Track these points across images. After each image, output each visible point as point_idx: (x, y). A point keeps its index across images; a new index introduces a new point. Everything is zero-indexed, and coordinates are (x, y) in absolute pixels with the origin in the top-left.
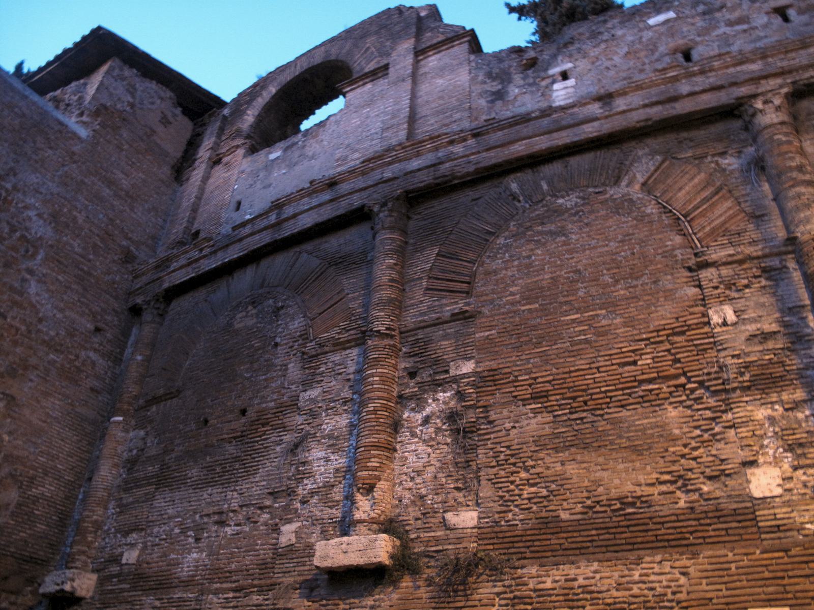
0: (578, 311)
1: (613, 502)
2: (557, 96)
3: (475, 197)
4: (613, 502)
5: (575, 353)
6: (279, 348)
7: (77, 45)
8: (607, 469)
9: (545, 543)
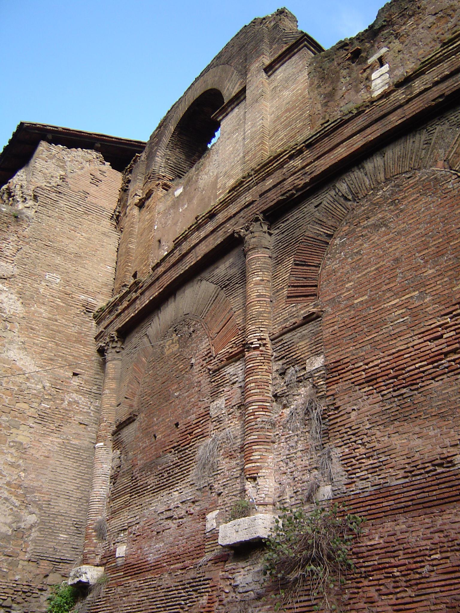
0: (396, 295)
1: (427, 465)
2: (376, 85)
3: (316, 204)
4: (427, 465)
5: (396, 336)
6: (195, 367)
7: (11, 142)
8: (422, 437)
9: (379, 506)
